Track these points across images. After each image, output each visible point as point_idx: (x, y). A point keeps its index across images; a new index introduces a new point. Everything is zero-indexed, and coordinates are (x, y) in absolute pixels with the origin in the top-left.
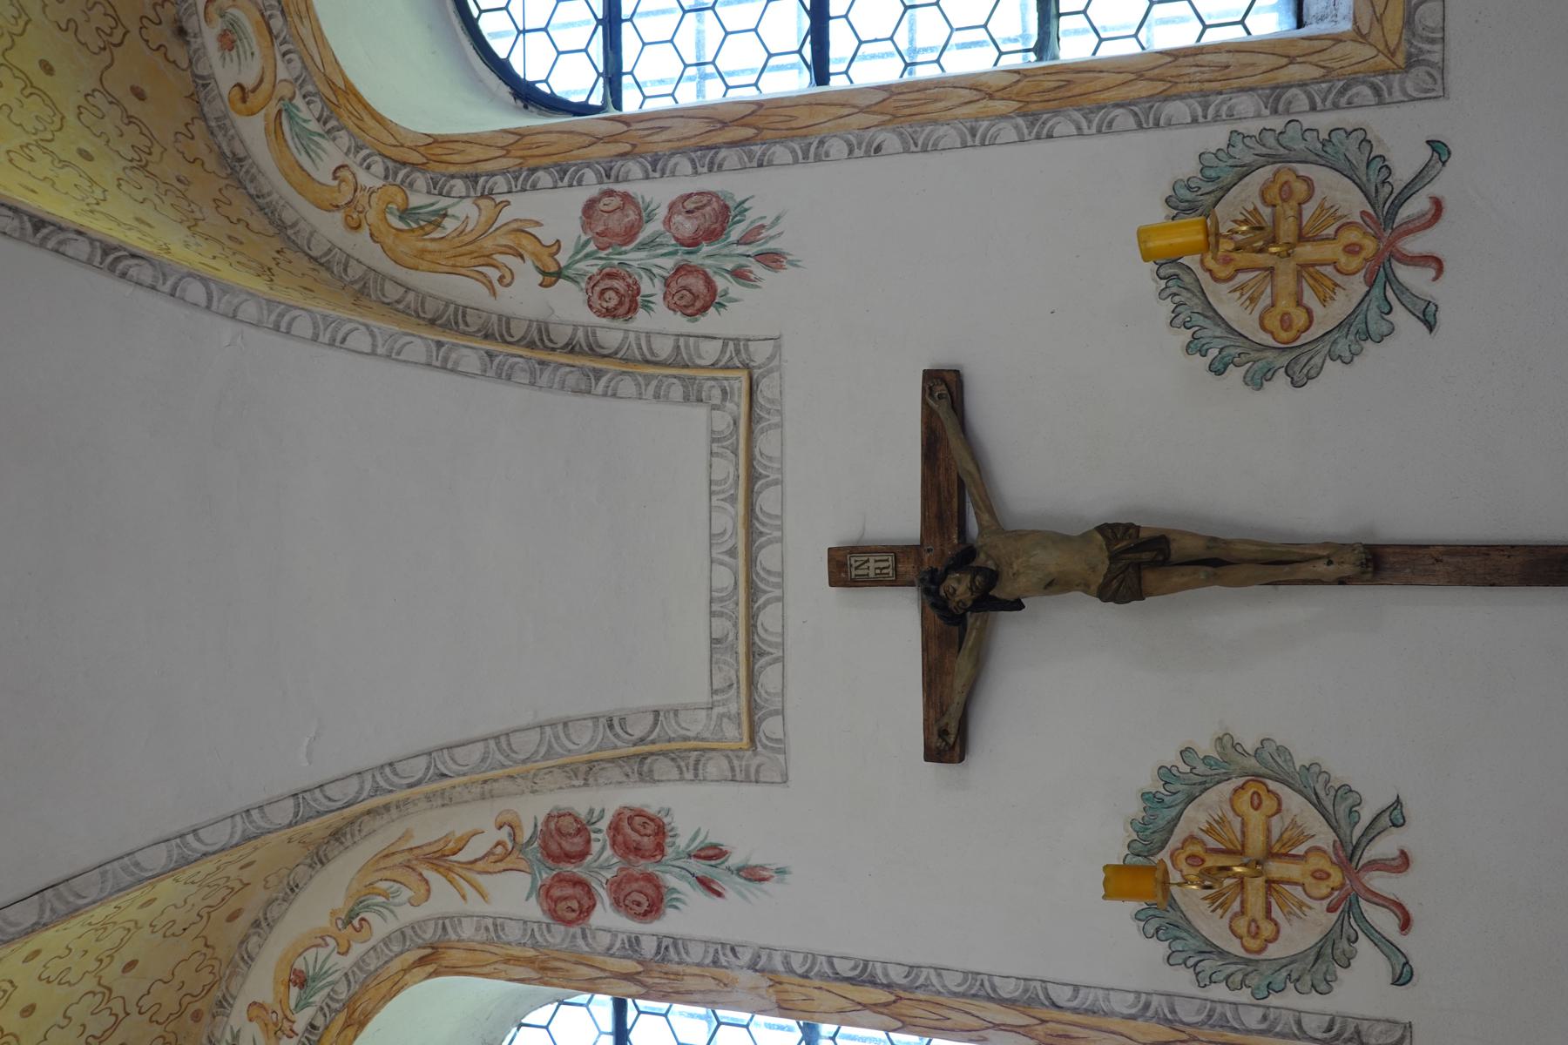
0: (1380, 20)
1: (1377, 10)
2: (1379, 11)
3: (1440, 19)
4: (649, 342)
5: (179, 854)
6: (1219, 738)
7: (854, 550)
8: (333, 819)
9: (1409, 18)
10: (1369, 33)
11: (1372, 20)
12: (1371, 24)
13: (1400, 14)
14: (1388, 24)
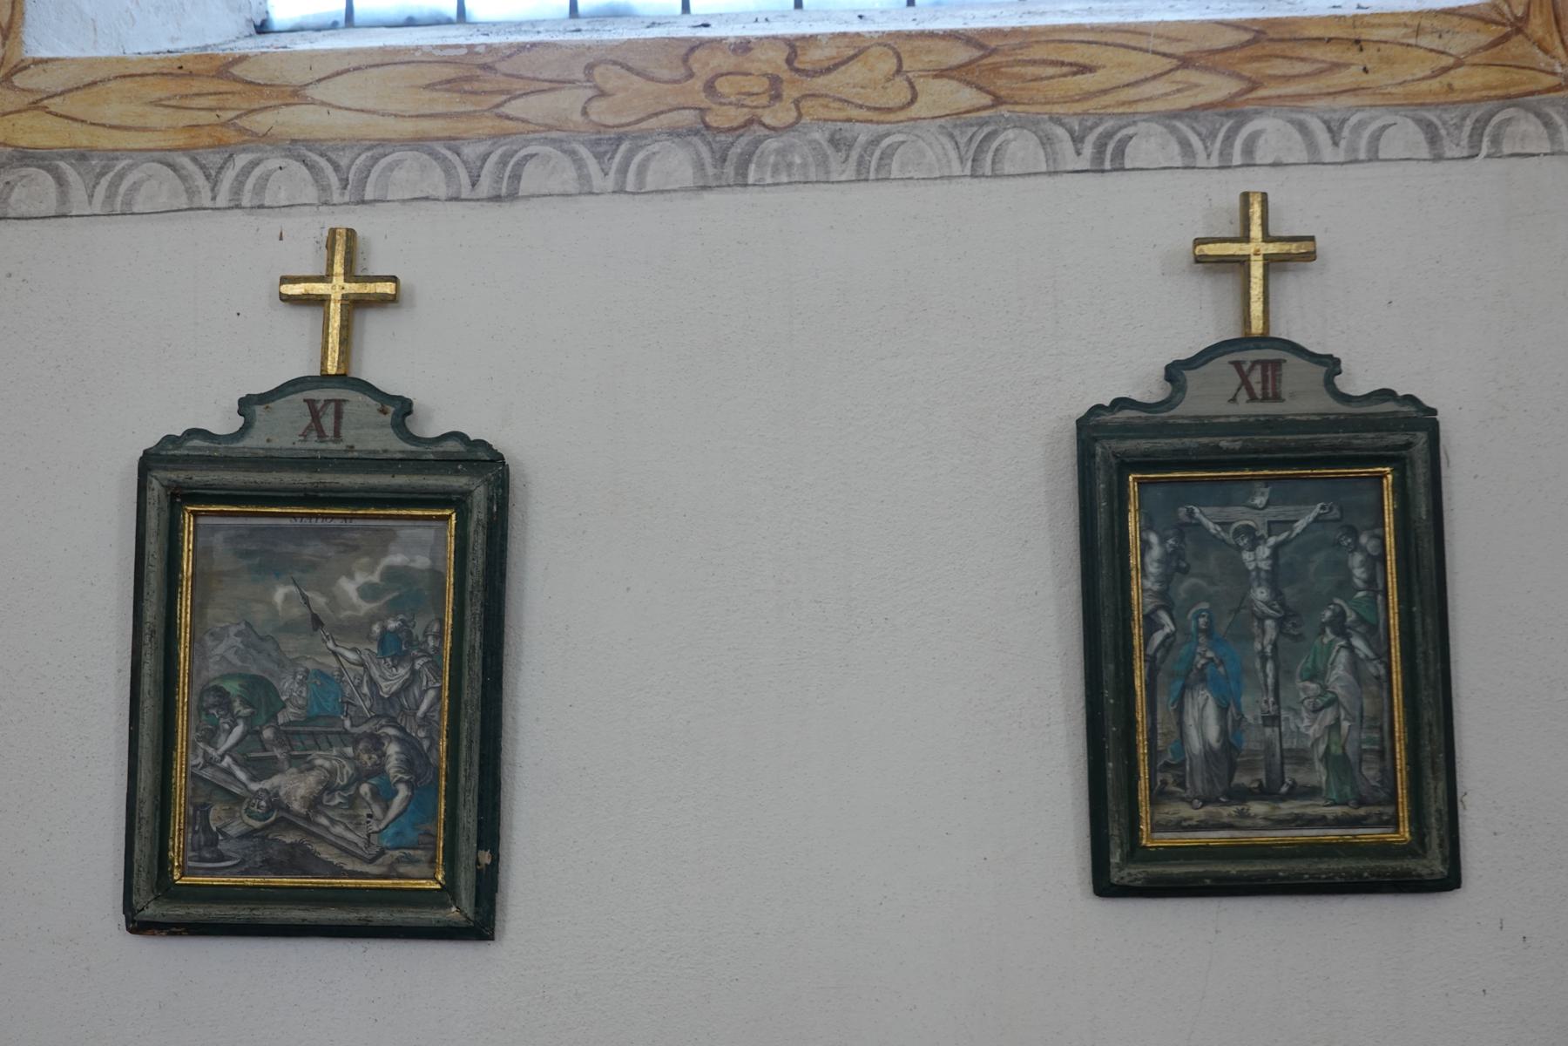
0: (35, 106)
1: (58, 100)
2: (55, 104)
3: (24, 210)
4: (324, 188)
5: (1102, 453)
6: (352, 447)
7: (129, 907)
8: (82, 137)
9: (33, 156)
10: (14, 88)
11: (38, 91)
12: (30, 91)
13: (42, 140)
14: (24, 120)
